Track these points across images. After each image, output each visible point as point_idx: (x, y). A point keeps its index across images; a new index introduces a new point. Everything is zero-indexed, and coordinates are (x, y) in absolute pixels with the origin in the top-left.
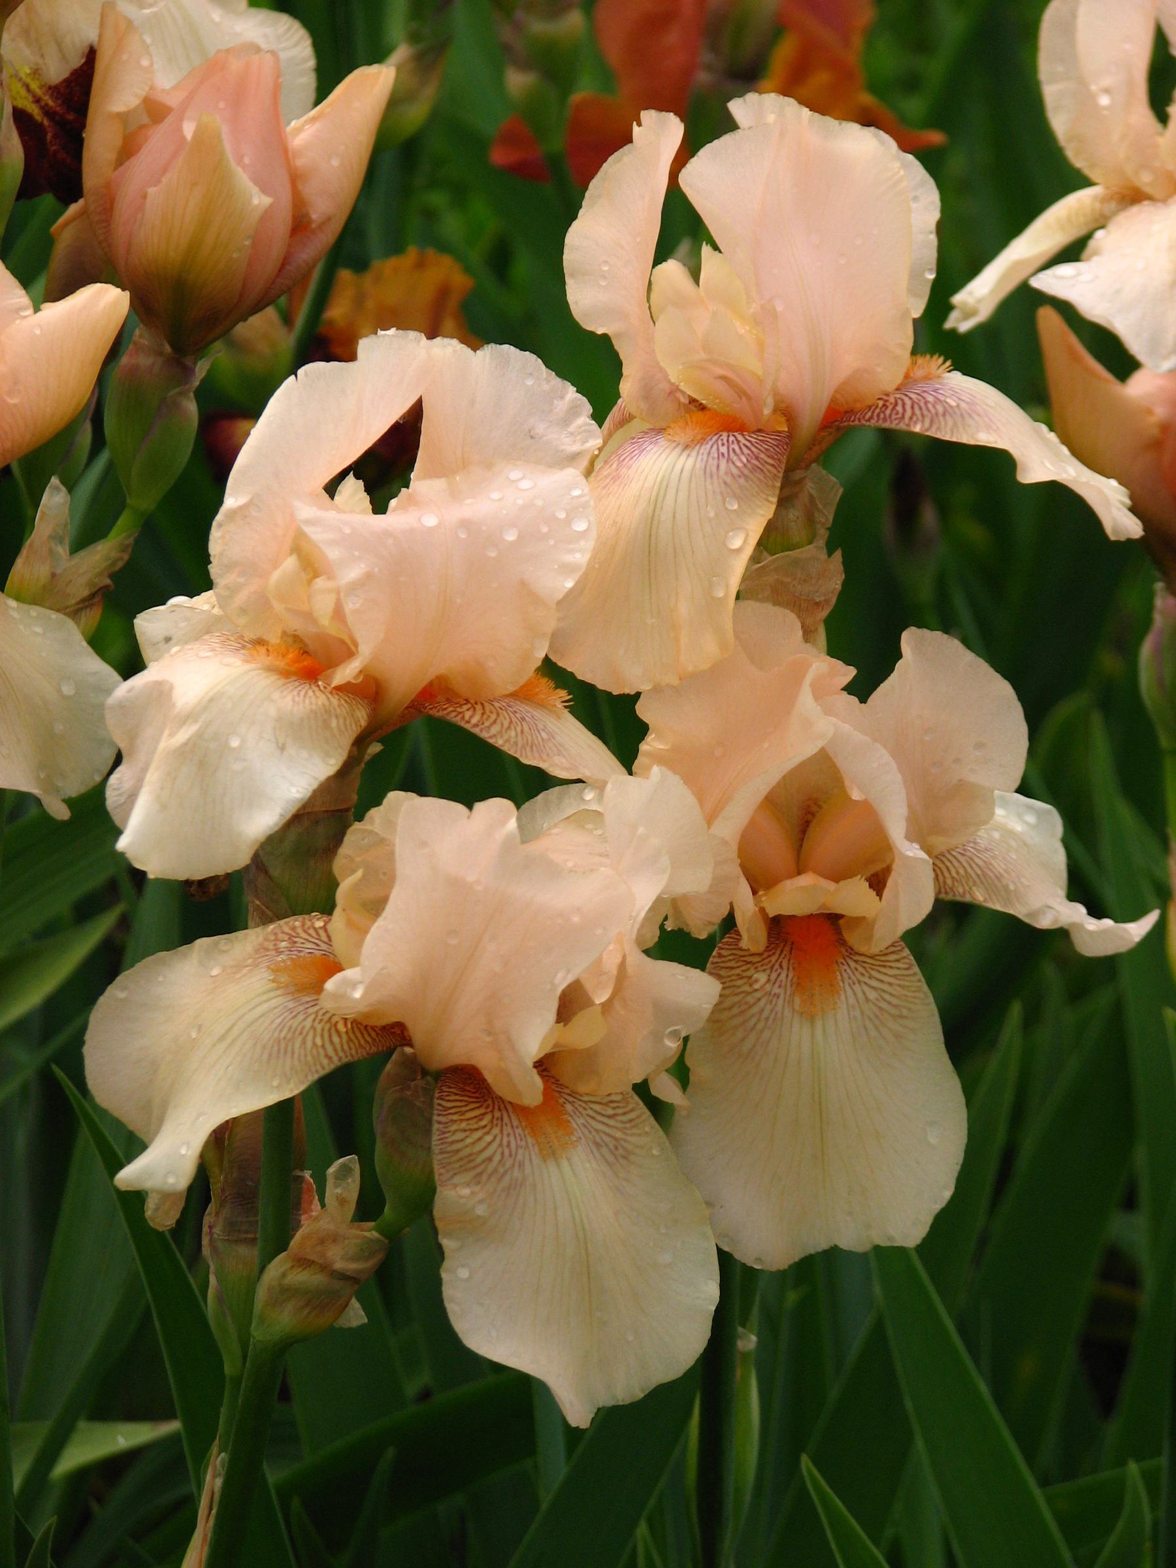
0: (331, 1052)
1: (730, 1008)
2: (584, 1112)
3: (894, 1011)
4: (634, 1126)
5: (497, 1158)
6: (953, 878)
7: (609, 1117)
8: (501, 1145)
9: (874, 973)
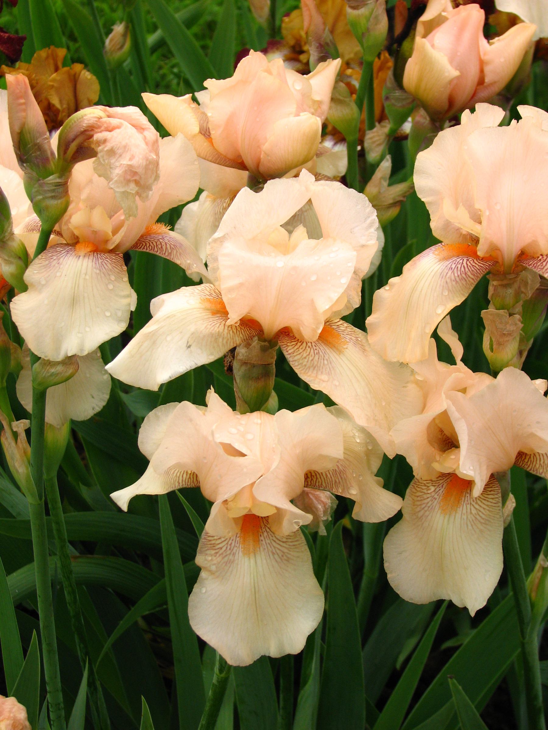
0: (180, 481)
1: (418, 497)
2: (271, 538)
3: (482, 521)
4: (296, 548)
5: (224, 549)
6: (540, 464)
7: (283, 542)
8: (227, 544)
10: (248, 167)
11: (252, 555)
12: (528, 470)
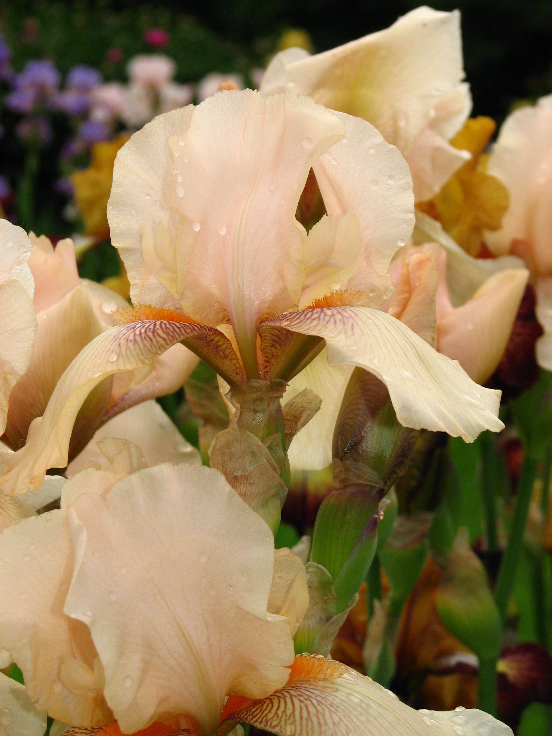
6: (276, 713)
10: (483, 158)
12: (251, 722)
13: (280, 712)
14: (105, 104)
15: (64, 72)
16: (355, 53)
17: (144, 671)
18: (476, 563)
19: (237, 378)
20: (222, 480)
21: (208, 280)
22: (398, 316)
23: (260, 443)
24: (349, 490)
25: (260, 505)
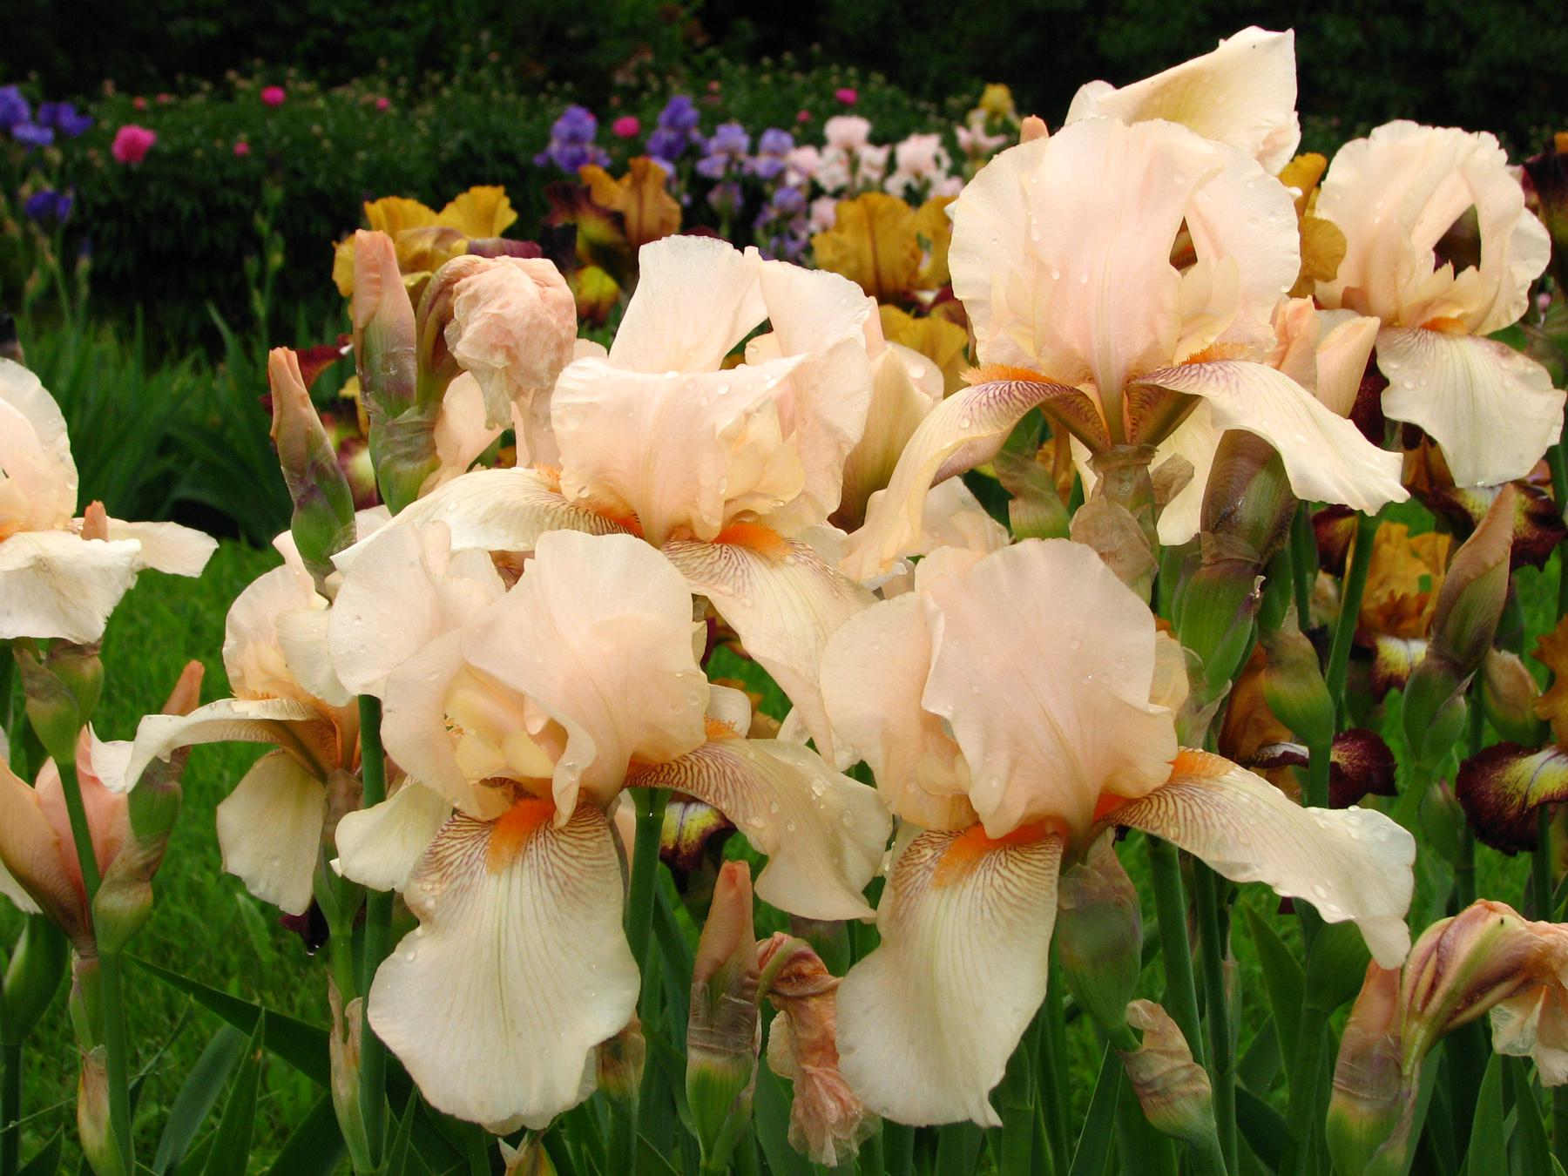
3: (1012, 900)
9: (1011, 866)
11: (505, 873)
13: (1161, 813)
14: (796, 168)
15: (755, 137)
16: (1176, 79)
17: (1012, 770)
18: (1307, 644)
19: (1098, 444)
20: (1095, 556)
21: (1070, 334)
22: (1277, 368)
23: (1129, 515)
24: (1222, 566)
25: (1133, 584)
